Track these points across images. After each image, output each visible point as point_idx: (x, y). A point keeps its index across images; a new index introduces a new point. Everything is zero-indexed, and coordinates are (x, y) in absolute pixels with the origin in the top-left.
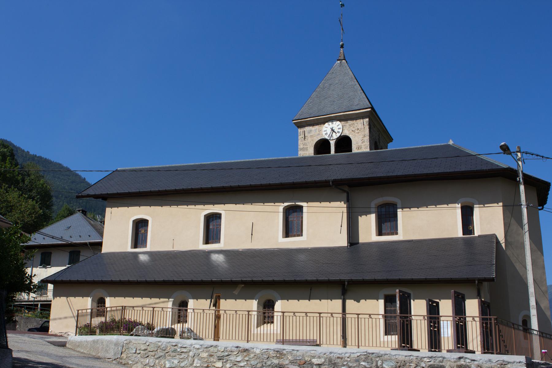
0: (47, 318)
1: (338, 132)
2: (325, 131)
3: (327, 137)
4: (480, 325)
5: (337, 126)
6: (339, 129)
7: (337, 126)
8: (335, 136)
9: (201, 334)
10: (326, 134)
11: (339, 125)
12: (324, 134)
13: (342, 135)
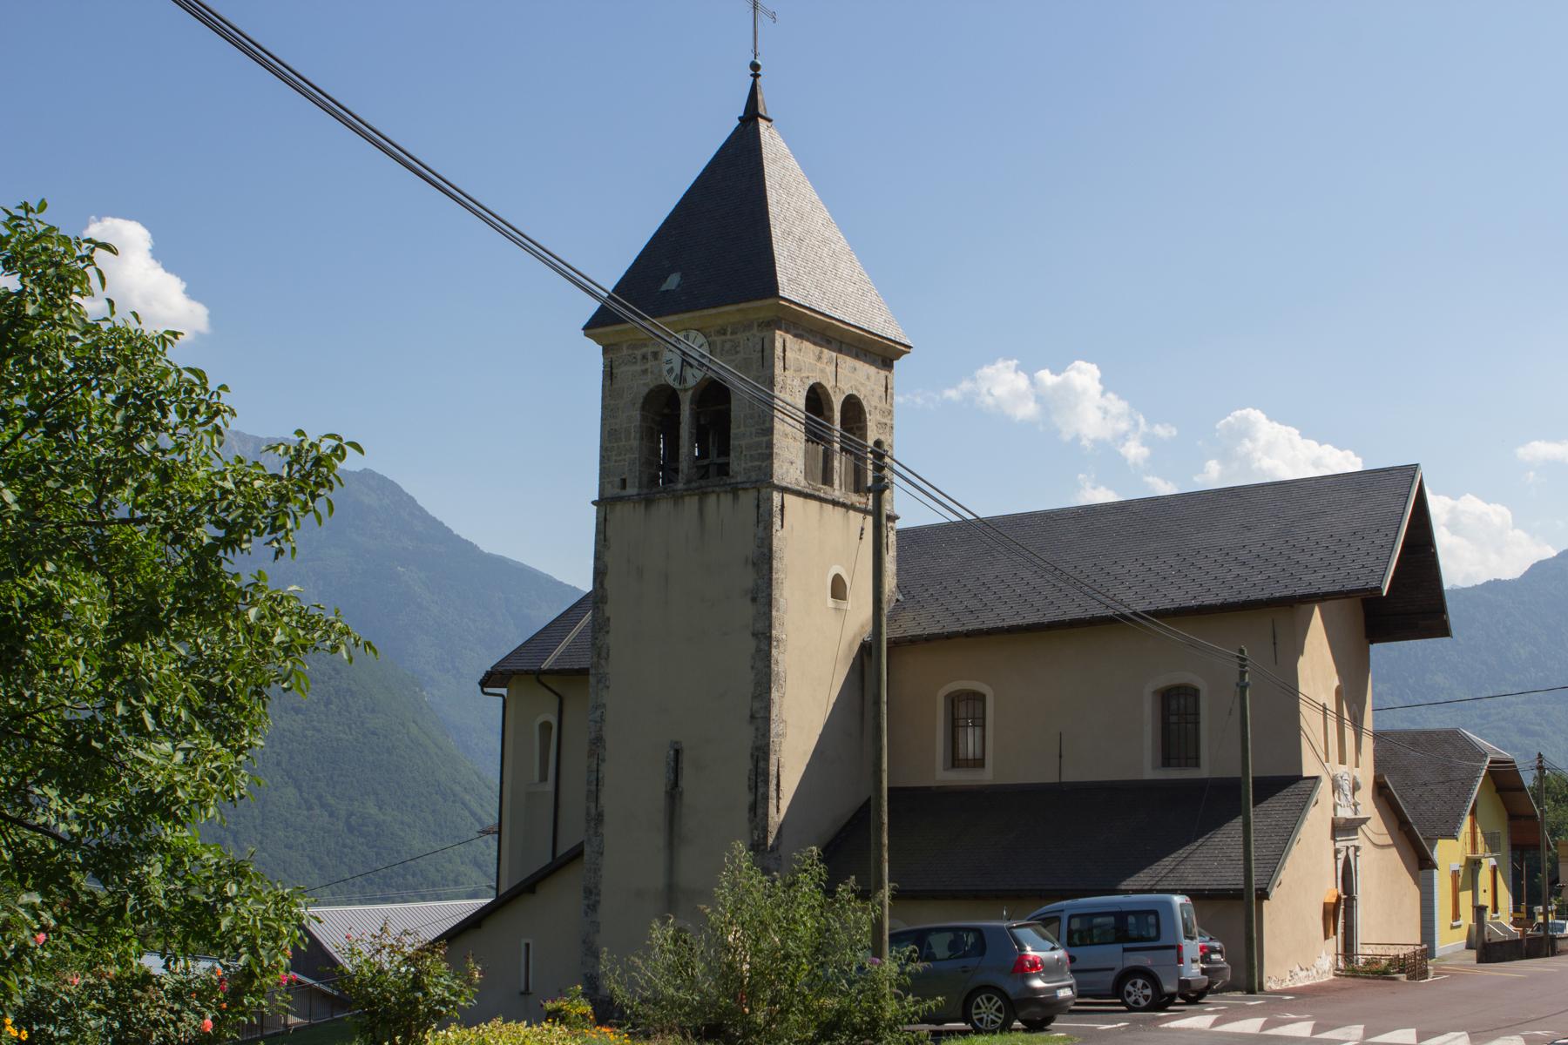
8: (694, 377)
10: (671, 371)
12: (665, 373)
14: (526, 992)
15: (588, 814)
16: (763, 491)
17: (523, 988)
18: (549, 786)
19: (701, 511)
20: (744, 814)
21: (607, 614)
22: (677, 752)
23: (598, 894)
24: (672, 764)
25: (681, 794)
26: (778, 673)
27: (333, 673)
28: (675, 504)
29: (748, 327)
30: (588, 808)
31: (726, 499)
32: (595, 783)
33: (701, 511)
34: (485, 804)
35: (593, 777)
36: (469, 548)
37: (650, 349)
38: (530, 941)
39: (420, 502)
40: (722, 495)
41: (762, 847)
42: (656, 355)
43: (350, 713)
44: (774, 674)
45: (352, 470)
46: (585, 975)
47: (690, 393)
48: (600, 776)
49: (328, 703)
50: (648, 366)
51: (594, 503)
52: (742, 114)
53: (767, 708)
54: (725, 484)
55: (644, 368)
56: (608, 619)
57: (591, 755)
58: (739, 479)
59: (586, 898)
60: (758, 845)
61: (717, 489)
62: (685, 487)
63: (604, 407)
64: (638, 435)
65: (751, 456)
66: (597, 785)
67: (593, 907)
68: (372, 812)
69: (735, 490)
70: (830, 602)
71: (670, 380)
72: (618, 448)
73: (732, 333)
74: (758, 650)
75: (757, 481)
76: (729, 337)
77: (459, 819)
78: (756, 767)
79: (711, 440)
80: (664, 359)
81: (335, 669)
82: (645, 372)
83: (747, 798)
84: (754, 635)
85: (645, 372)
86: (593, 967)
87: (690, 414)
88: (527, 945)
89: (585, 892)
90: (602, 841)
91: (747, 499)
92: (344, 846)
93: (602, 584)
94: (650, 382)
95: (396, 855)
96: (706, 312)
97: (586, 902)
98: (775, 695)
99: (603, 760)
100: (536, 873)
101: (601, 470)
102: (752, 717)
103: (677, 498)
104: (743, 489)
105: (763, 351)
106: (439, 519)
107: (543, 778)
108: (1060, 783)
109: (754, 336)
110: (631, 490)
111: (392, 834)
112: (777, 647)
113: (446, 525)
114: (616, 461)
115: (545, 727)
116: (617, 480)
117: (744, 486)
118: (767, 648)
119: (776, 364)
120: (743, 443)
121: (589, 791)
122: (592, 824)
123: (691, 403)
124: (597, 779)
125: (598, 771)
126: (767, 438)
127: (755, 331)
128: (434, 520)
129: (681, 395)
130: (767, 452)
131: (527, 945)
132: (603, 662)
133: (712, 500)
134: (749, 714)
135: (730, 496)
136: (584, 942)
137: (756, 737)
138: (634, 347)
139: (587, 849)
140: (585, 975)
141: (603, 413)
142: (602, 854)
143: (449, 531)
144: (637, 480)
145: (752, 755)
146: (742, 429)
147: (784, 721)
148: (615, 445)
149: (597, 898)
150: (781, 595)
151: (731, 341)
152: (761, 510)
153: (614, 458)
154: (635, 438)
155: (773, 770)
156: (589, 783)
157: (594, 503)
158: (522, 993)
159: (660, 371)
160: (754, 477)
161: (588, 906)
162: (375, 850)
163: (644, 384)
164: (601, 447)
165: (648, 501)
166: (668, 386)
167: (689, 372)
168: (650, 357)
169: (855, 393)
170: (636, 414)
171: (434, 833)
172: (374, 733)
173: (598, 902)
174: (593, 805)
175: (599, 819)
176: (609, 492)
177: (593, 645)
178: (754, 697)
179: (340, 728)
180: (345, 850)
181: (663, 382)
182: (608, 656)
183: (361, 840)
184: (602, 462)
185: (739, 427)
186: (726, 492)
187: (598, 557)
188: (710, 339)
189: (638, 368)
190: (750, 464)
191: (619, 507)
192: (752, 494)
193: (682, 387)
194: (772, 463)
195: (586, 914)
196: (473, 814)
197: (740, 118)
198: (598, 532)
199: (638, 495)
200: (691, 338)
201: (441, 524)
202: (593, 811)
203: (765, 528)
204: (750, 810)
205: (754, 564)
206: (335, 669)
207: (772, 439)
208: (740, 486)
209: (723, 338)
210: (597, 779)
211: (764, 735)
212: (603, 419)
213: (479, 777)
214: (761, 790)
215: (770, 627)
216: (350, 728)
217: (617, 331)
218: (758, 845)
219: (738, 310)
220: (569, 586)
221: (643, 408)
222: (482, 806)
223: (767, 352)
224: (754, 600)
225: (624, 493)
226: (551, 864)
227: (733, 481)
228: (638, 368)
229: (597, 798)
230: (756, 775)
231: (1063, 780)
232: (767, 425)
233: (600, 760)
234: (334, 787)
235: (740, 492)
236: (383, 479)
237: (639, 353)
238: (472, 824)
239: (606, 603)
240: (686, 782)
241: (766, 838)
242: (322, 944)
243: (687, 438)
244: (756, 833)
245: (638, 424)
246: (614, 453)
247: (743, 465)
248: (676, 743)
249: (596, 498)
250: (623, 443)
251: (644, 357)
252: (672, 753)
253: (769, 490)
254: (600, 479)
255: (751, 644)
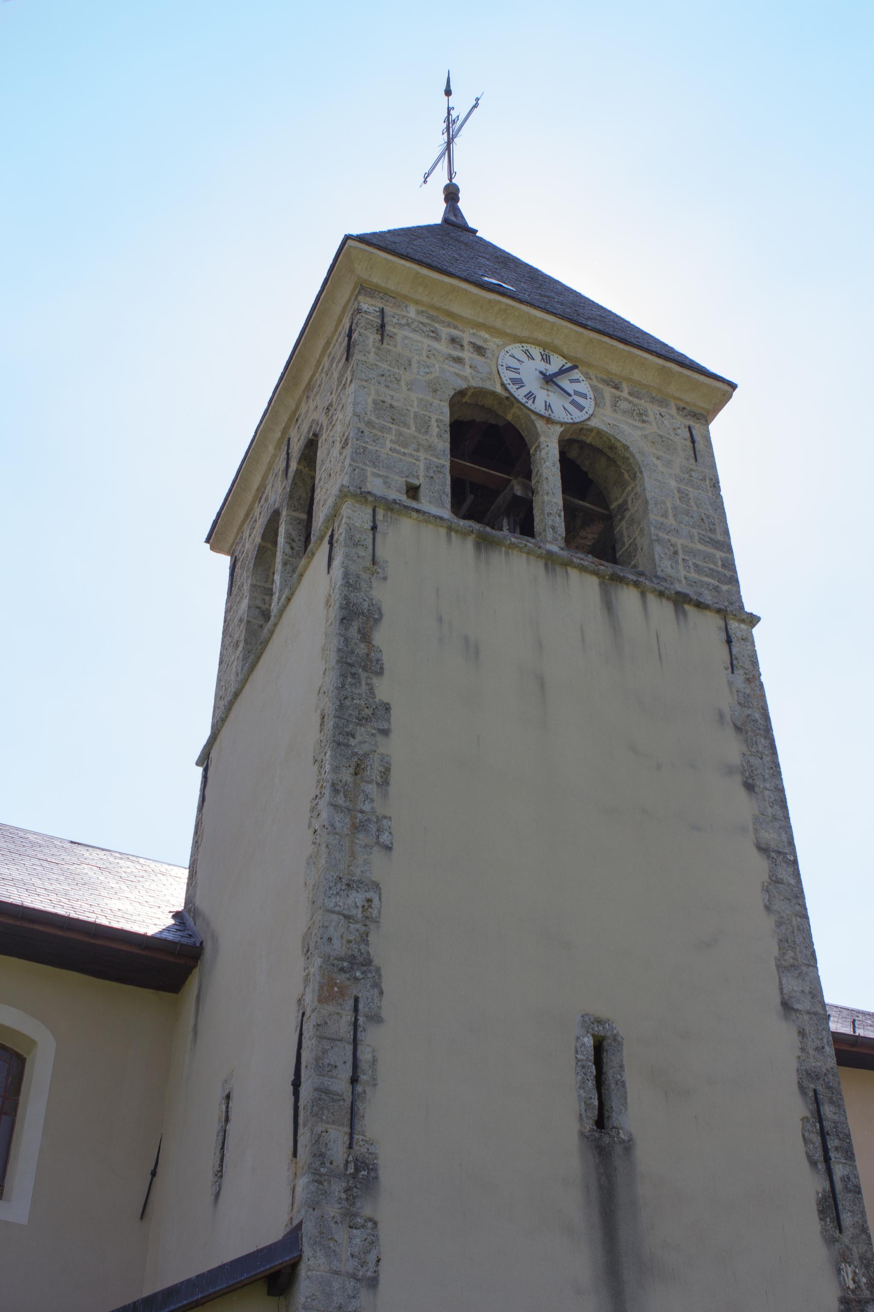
25: (628, 1147)
48: (365, 1056)
74: (776, 881)
90: (372, 1242)
99: (376, 1019)
108: (189, 868)
118: (793, 882)
122: (337, 1188)
125: (355, 1042)
134: (778, 1000)
142: (373, 1283)
145: (802, 1089)
178: (783, 968)
204: (822, 1212)
223: (700, 445)
224: (750, 787)
229: (353, 1113)
231: (188, 867)
255: (760, 866)
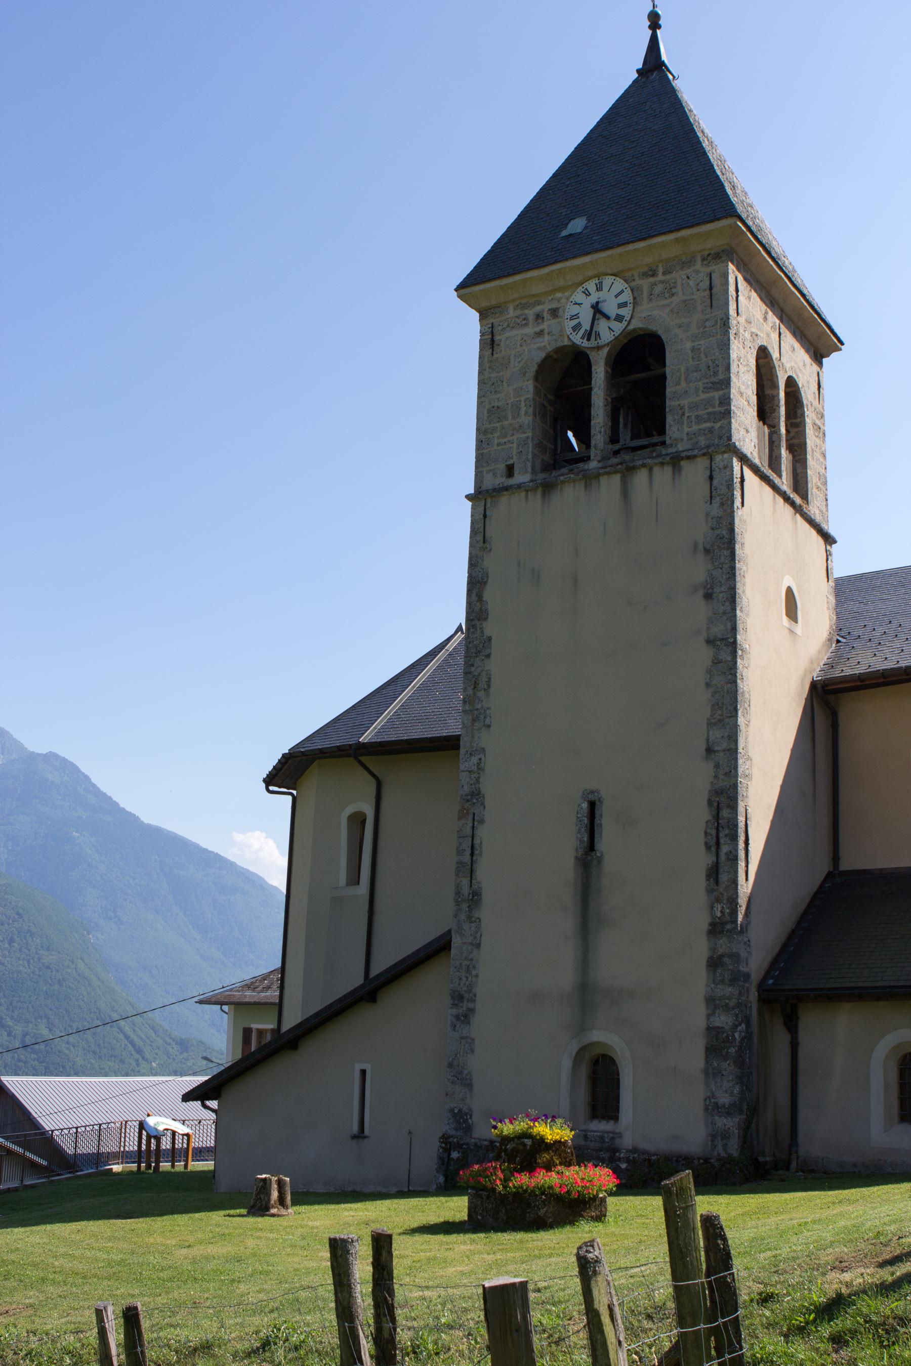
0: (45, 1073)
1: (619, 318)
2: (572, 318)
3: (577, 339)
4: (187, 839)
5: (616, 296)
6: (622, 305)
7: (616, 296)
8: (608, 332)
9: (190, 1105)
10: (577, 328)
11: (622, 291)
12: (569, 331)
13: (631, 327)
14: (360, 1135)
15: (458, 893)
16: (718, 458)
17: (355, 1128)
18: (363, 889)
19: (625, 493)
20: (700, 882)
21: (487, 633)
22: (592, 805)
23: (472, 1000)
24: (586, 821)
25: (600, 860)
26: (743, 693)
27: (16, 917)
28: (586, 486)
29: (690, 262)
30: (458, 887)
31: (663, 475)
32: (468, 852)
33: (625, 493)
34: (137, 1029)
35: (467, 844)
36: (131, 819)
37: (546, 307)
38: (367, 1067)
39: (94, 780)
40: (656, 470)
41: (728, 927)
42: (554, 313)
43: (29, 950)
44: (740, 691)
45: (40, 752)
46: (452, 1110)
47: (606, 350)
48: (477, 841)
49: (11, 941)
50: (544, 326)
51: (468, 497)
52: (640, 66)
53: (733, 736)
54: (659, 456)
55: (538, 329)
56: (490, 639)
57: (462, 816)
58: (680, 447)
59: (454, 1005)
60: (723, 924)
61: (649, 461)
62: (600, 465)
63: (481, 383)
64: (531, 410)
65: (697, 417)
66: (472, 854)
67: (465, 1018)
68: (43, 1033)
69: (676, 461)
70: (785, 621)
71: (577, 339)
72: (503, 427)
73: (664, 274)
74: (716, 662)
75: (708, 447)
76: (660, 277)
77: (115, 1041)
78: (717, 817)
79: (621, 420)
80: (567, 315)
81: (18, 914)
82: (540, 334)
83: (704, 860)
84: (709, 642)
85: (540, 334)
86: (463, 1100)
87: (605, 376)
88: (363, 1072)
89: (453, 998)
90: (479, 928)
91: (695, 472)
92: (19, 1060)
93: (480, 597)
94: (547, 344)
95: (61, 1069)
96: (630, 247)
97: (454, 1011)
98: (741, 720)
99: (482, 821)
100: (418, 951)
101: (477, 458)
102: (709, 750)
103: (590, 479)
104: (689, 458)
105: (711, 289)
106: (109, 794)
107: (354, 880)
109: (697, 272)
110: (521, 477)
111: (59, 1052)
112: (742, 659)
113: (114, 799)
114: (498, 445)
115: (357, 820)
116: (501, 467)
117: (689, 453)
118: (729, 658)
119: (731, 303)
120: (685, 402)
121: (460, 863)
122: (465, 906)
123: (606, 364)
124: (472, 847)
126: (721, 393)
127: (698, 265)
128: (105, 795)
129: (592, 356)
130: (722, 409)
131: (363, 1072)
132: (481, 694)
133: (640, 478)
135: (668, 470)
136: (450, 1065)
137: (716, 777)
138: (524, 307)
139: (456, 941)
140: (452, 1110)
141: (480, 389)
142: (478, 946)
143: (116, 804)
144: (529, 465)
145: (710, 802)
146: (683, 384)
147: (749, 759)
148: (498, 425)
149: (471, 1005)
150: (744, 592)
151: (662, 282)
152: (715, 482)
153: (496, 441)
154: (526, 414)
155: (741, 819)
156: (460, 852)
157: (468, 497)
158: (354, 1137)
159: (562, 330)
160: (702, 441)
161: (457, 1017)
162: (44, 1064)
163: (539, 348)
164: (478, 429)
165: (547, 488)
166: (574, 345)
167: (603, 326)
168: (546, 315)
169: (794, 376)
170: (529, 386)
171: (94, 1052)
172: (48, 967)
173: (472, 1011)
174: (465, 882)
175: (475, 898)
176: (490, 482)
177: (466, 673)
178: (711, 725)
179: (21, 962)
180: (20, 1064)
181: (566, 342)
182: (489, 686)
183: (33, 1056)
184: (478, 448)
185: (678, 383)
186: (662, 464)
187: (474, 563)
188: (633, 284)
189: (530, 330)
190: (695, 427)
191: (504, 500)
192: (703, 462)
193: (593, 343)
194: (730, 423)
195: (454, 1027)
196: (127, 1037)
197: (638, 71)
198: (474, 532)
199: (532, 481)
200: (606, 287)
201: (110, 798)
202: (466, 890)
203: (722, 504)
205: (707, 551)
206: (18, 914)
207: (729, 393)
208: (683, 454)
209: (651, 280)
210: (472, 847)
211: (727, 774)
212: (480, 397)
213: (133, 1007)
214: (725, 849)
215: (734, 629)
216: (29, 963)
217: (501, 287)
218: (723, 924)
219: (677, 240)
220: (213, 852)
221: (536, 378)
222: (134, 1030)
224: (708, 596)
225: (511, 482)
226: (361, 987)
227: (670, 450)
228: (530, 330)
229: (472, 871)
230: (717, 829)
232: (721, 377)
233: (476, 821)
234: (13, 1011)
235: (682, 463)
236: (64, 760)
237: (531, 313)
238: (125, 1045)
239: (486, 619)
240: (604, 845)
241: (734, 912)
242: (30, 1114)
243: (601, 404)
244: (718, 907)
245: (530, 396)
246: (496, 435)
247: (686, 429)
248: (592, 792)
249: (471, 490)
250: (510, 421)
251: (539, 317)
252: (585, 805)
253: (726, 456)
254: (477, 467)
255: (706, 655)
